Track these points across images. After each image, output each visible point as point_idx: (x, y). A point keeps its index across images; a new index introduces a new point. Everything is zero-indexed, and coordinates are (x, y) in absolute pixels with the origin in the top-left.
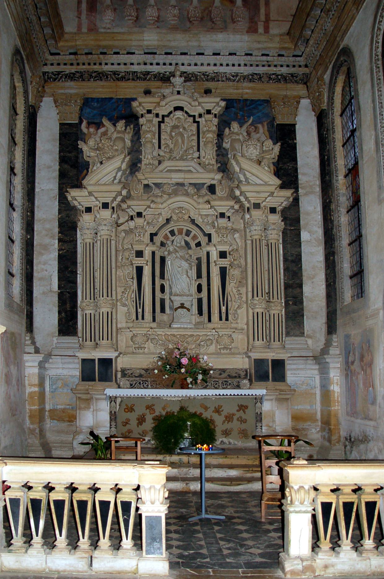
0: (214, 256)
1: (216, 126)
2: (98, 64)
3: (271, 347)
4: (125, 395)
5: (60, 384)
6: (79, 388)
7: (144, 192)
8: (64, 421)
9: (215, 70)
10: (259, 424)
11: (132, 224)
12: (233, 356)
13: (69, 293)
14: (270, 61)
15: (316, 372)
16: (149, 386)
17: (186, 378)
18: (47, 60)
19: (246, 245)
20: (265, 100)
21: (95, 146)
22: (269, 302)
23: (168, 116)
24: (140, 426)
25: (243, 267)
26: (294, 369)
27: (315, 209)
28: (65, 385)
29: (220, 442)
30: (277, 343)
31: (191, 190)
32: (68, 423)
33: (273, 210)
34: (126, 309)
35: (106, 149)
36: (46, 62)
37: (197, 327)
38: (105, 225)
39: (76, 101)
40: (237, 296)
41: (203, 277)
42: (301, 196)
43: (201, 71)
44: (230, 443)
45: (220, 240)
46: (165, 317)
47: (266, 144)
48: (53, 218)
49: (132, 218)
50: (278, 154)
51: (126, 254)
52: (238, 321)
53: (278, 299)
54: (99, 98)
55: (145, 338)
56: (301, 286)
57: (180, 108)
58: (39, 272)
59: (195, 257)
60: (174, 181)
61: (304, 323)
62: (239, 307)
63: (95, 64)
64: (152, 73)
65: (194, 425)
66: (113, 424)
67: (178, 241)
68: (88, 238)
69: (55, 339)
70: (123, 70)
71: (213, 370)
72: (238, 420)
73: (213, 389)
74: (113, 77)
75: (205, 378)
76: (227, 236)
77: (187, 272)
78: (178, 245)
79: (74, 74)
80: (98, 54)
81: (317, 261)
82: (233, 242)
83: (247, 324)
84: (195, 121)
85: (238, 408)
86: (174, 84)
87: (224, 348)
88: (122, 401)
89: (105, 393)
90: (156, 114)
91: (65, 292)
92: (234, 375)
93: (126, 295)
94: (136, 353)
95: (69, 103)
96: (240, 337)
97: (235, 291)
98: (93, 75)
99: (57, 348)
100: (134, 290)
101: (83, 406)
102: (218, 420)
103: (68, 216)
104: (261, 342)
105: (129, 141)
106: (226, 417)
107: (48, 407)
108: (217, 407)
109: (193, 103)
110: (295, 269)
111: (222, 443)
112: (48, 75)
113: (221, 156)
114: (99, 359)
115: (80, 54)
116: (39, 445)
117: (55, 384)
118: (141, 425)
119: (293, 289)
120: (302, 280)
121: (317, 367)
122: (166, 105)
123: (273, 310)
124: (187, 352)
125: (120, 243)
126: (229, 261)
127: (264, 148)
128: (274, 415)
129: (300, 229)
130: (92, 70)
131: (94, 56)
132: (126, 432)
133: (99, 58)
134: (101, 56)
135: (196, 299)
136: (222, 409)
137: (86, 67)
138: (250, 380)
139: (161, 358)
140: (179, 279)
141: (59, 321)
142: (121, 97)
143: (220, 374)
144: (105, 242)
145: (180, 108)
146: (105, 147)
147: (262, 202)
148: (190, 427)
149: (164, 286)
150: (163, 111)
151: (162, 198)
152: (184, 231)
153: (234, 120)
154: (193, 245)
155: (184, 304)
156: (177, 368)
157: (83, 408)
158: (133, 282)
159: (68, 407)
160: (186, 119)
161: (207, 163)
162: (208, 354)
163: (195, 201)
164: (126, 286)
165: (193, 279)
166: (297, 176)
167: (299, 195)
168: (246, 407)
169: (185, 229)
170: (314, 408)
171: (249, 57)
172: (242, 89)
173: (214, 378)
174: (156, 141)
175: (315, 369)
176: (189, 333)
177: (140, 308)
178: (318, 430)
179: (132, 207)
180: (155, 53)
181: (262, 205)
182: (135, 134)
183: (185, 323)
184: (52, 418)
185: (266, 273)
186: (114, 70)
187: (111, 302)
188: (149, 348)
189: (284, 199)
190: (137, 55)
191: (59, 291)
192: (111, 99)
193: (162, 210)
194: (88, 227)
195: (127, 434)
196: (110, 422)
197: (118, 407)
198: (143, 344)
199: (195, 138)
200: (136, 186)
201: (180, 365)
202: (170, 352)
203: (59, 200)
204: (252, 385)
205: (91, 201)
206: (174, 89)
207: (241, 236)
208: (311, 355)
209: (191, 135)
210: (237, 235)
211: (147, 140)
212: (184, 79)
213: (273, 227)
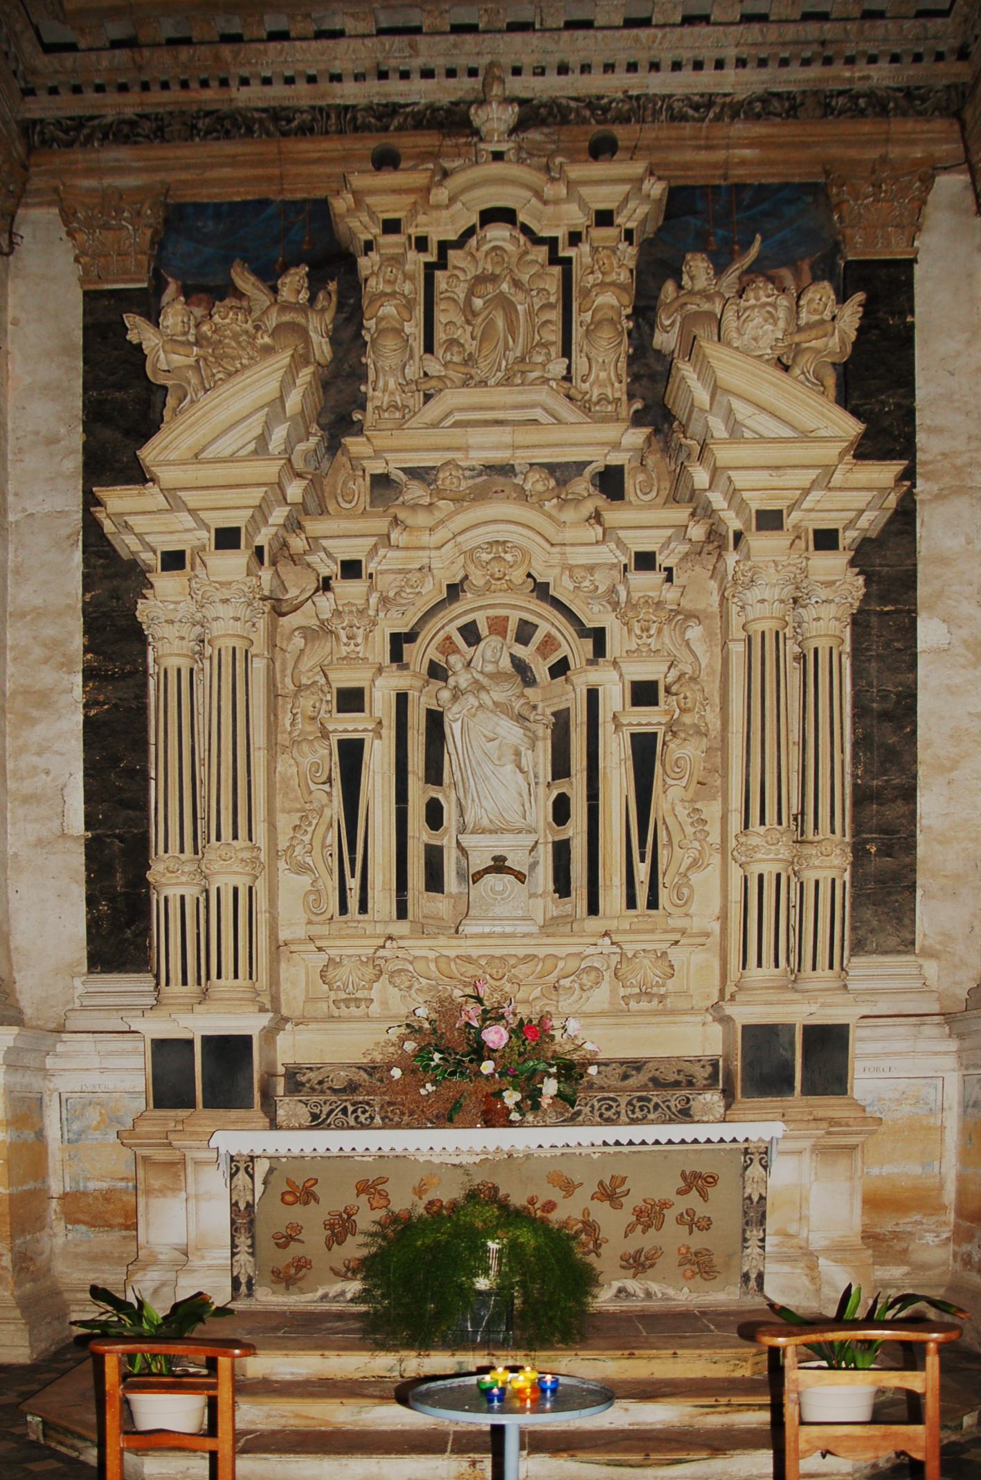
0: (614, 698)
1: (631, 271)
2: (214, 84)
3: (801, 985)
4: (283, 1152)
5: (93, 1116)
6: (144, 1128)
7: (371, 502)
8: (111, 1226)
9: (633, 88)
10: (754, 1234)
11: (325, 603)
12: (671, 1019)
13: (121, 839)
14: (832, 42)
15: (950, 1062)
16: (378, 1120)
17: (502, 1091)
18: (35, 72)
19: (726, 662)
20: (801, 185)
21: (185, 333)
22: (801, 842)
23: (460, 243)
24: (335, 1245)
25: (713, 734)
26: (876, 1056)
27: (968, 543)
28: (110, 1119)
29: (614, 1291)
30: (823, 971)
31: (536, 483)
32: (124, 1233)
33: (826, 540)
34: (306, 880)
35: (229, 346)
36: (29, 78)
37: (550, 930)
38: (226, 601)
39: (139, 214)
40: (690, 830)
41: (573, 772)
42: (922, 501)
43: (582, 93)
44: (649, 1295)
45: (634, 647)
46: (440, 905)
47: (811, 301)
48: (68, 606)
49: (325, 585)
50: (853, 336)
51: (306, 703)
52: (691, 911)
53: (833, 832)
54: (222, 204)
55: (370, 971)
56: (909, 794)
57: (506, 215)
58: (22, 779)
59: (549, 711)
60: (478, 457)
61: (914, 910)
62: (695, 864)
63: (204, 84)
64: (409, 109)
65: (513, 1251)
66: (243, 1241)
67: (489, 654)
68: (171, 655)
69: (78, 982)
70: (305, 103)
71: (599, 1064)
72: (680, 1220)
73: (600, 1125)
74: (271, 127)
75: (568, 1091)
76: (660, 631)
77: (518, 754)
78: (490, 668)
79: (132, 124)
80: (211, 43)
81: (970, 714)
82: (683, 654)
83: (724, 917)
84: (554, 259)
85: (681, 1184)
86: (484, 130)
87: (645, 994)
88: (271, 1170)
89: (212, 1144)
90: (417, 239)
91: (108, 836)
92: (672, 1077)
93: (309, 836)
94: (339, 1019)
95: (114, 218)
96: (698, 957)
97: (682, 812)
98: (200, 125)
99: (84, 1008)
100: (335, 818)
101: (156, 1184)
102: (611, 1221)
103: (115, 595)
104: (768, 969)
105: (325, 340)
106: (639, 1213)
107: (56, 1186)
108: (607, 1182)
109: (549, 191)
110: (892, 740)
111: (623, 1295)
112: (42, 133)
113: (644, 382)
114: (206, 1040)
115: (148, 46)
116: (13, 1303)
117: (78, 1118)
118: (339, 1244)
119: (882, 805)
120: (915, 777)
121: (953, 1045)
122: (452, 199)
123: (816, 867)
124: (507, 1010)
125: (289, 672)
126: (666, 712)
127: (803, 315)
128: (804, 1199)
129: (915, 611)
130: (195, 108)
131: (203, 51)
132: (288, 1266)
133: (217, 58)
134: (226, 51)
135: (550, 846)
136: (624, 1188)
137: (175, 95)
138: (728, 1094)
139: (413, 1030)
140: (487, 778)
141: (89, 927)
142: (300, 196)
143: (625, 1077)
144: (227, 659)
145: (506, 215)
146: (225, 337)
147: (791, 508)
148: (500, 1259)
149: (441, 808)
150: (442, 228)
151: (431, 512)
152: (512, 626)
153: (696, 250)
154: (541, 670)
155: (504, 859)
156: (471, 1061)
157: (161, 1191)
158: (329, 794)
159: (123, 1184)
160: (526, 253)
161: (594, 399)
162: (587, 1015)
163: (550, 517)
164: (307, 806)
165: (541, 780)
166: (912, 435)
167: (918, 498)
168: (712, 1180)
169: (514, 617)
170: (936, 1170)
171: (756, 27)
172: (728, 147)
173: (602, 1089)
174: (414, 329)
175: (946, 1053)
176: (522, 952)
177: (353, 876)
178: (945, 1236)
179: (325, 543)
180: (417, 30)
181: (789, 522)
182: (348, 320)
183: (507, 919)
184: (71, 1219)
185: (795, 753)
186: (273, 104)
187: (246, 855)
188: (384, 1003)
189: (867, 496)
190: (351, 40)
191: (89, 834)
192: (263, 203)
193: (434, 553)
194: (171, 617)
195: (293, 1271)
196: (233, 1237)
197: (259, 1188)
198: (364, 988)
199: (555, 315)
200: (345, 483)
201: (480, 1051)
202: (447, 1009)
203: (84, 546)
204: (734, 1106)
205: (180, 528)
206: (482, 146)
207: (710, 634)
208: (935, 1008)
209: (542, 308)
210: (695, 632)
211: (383, 324)
212: (517, 109)
213: (823, 594)
